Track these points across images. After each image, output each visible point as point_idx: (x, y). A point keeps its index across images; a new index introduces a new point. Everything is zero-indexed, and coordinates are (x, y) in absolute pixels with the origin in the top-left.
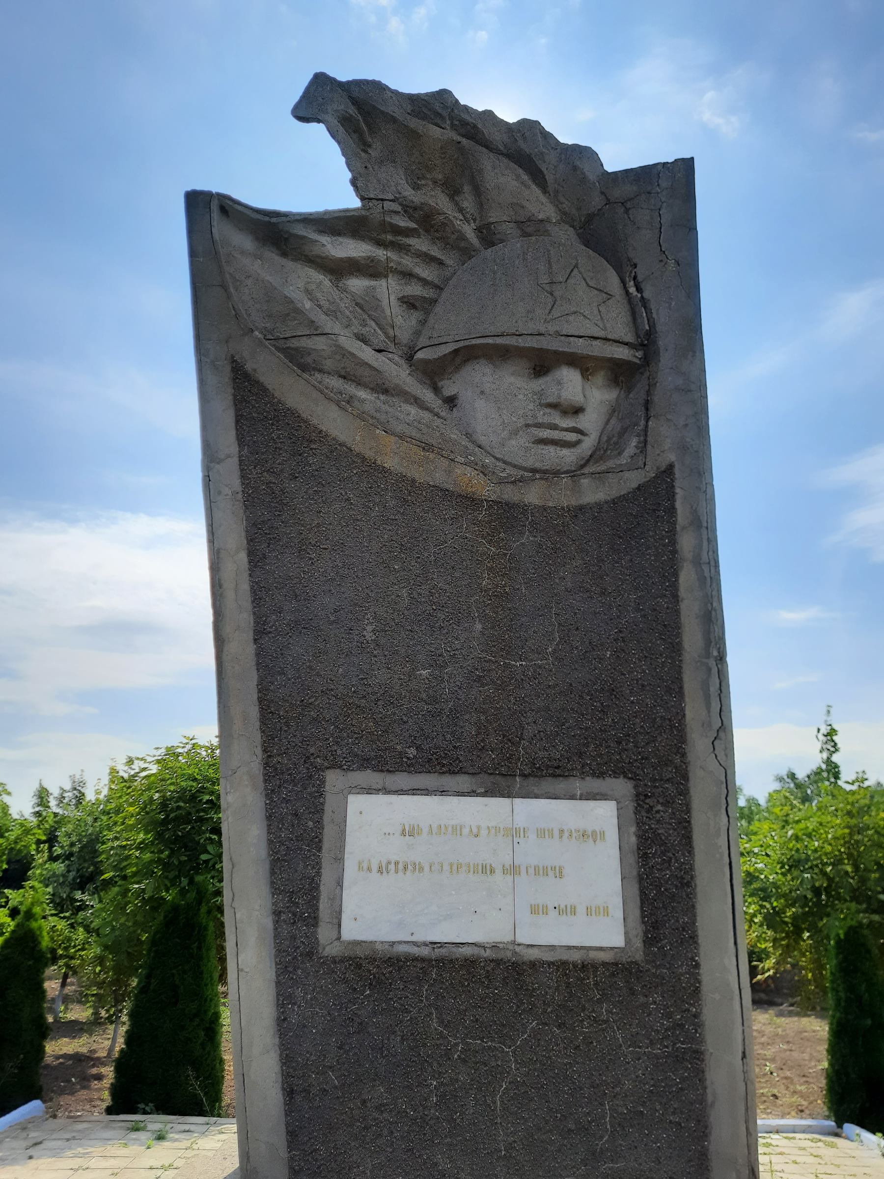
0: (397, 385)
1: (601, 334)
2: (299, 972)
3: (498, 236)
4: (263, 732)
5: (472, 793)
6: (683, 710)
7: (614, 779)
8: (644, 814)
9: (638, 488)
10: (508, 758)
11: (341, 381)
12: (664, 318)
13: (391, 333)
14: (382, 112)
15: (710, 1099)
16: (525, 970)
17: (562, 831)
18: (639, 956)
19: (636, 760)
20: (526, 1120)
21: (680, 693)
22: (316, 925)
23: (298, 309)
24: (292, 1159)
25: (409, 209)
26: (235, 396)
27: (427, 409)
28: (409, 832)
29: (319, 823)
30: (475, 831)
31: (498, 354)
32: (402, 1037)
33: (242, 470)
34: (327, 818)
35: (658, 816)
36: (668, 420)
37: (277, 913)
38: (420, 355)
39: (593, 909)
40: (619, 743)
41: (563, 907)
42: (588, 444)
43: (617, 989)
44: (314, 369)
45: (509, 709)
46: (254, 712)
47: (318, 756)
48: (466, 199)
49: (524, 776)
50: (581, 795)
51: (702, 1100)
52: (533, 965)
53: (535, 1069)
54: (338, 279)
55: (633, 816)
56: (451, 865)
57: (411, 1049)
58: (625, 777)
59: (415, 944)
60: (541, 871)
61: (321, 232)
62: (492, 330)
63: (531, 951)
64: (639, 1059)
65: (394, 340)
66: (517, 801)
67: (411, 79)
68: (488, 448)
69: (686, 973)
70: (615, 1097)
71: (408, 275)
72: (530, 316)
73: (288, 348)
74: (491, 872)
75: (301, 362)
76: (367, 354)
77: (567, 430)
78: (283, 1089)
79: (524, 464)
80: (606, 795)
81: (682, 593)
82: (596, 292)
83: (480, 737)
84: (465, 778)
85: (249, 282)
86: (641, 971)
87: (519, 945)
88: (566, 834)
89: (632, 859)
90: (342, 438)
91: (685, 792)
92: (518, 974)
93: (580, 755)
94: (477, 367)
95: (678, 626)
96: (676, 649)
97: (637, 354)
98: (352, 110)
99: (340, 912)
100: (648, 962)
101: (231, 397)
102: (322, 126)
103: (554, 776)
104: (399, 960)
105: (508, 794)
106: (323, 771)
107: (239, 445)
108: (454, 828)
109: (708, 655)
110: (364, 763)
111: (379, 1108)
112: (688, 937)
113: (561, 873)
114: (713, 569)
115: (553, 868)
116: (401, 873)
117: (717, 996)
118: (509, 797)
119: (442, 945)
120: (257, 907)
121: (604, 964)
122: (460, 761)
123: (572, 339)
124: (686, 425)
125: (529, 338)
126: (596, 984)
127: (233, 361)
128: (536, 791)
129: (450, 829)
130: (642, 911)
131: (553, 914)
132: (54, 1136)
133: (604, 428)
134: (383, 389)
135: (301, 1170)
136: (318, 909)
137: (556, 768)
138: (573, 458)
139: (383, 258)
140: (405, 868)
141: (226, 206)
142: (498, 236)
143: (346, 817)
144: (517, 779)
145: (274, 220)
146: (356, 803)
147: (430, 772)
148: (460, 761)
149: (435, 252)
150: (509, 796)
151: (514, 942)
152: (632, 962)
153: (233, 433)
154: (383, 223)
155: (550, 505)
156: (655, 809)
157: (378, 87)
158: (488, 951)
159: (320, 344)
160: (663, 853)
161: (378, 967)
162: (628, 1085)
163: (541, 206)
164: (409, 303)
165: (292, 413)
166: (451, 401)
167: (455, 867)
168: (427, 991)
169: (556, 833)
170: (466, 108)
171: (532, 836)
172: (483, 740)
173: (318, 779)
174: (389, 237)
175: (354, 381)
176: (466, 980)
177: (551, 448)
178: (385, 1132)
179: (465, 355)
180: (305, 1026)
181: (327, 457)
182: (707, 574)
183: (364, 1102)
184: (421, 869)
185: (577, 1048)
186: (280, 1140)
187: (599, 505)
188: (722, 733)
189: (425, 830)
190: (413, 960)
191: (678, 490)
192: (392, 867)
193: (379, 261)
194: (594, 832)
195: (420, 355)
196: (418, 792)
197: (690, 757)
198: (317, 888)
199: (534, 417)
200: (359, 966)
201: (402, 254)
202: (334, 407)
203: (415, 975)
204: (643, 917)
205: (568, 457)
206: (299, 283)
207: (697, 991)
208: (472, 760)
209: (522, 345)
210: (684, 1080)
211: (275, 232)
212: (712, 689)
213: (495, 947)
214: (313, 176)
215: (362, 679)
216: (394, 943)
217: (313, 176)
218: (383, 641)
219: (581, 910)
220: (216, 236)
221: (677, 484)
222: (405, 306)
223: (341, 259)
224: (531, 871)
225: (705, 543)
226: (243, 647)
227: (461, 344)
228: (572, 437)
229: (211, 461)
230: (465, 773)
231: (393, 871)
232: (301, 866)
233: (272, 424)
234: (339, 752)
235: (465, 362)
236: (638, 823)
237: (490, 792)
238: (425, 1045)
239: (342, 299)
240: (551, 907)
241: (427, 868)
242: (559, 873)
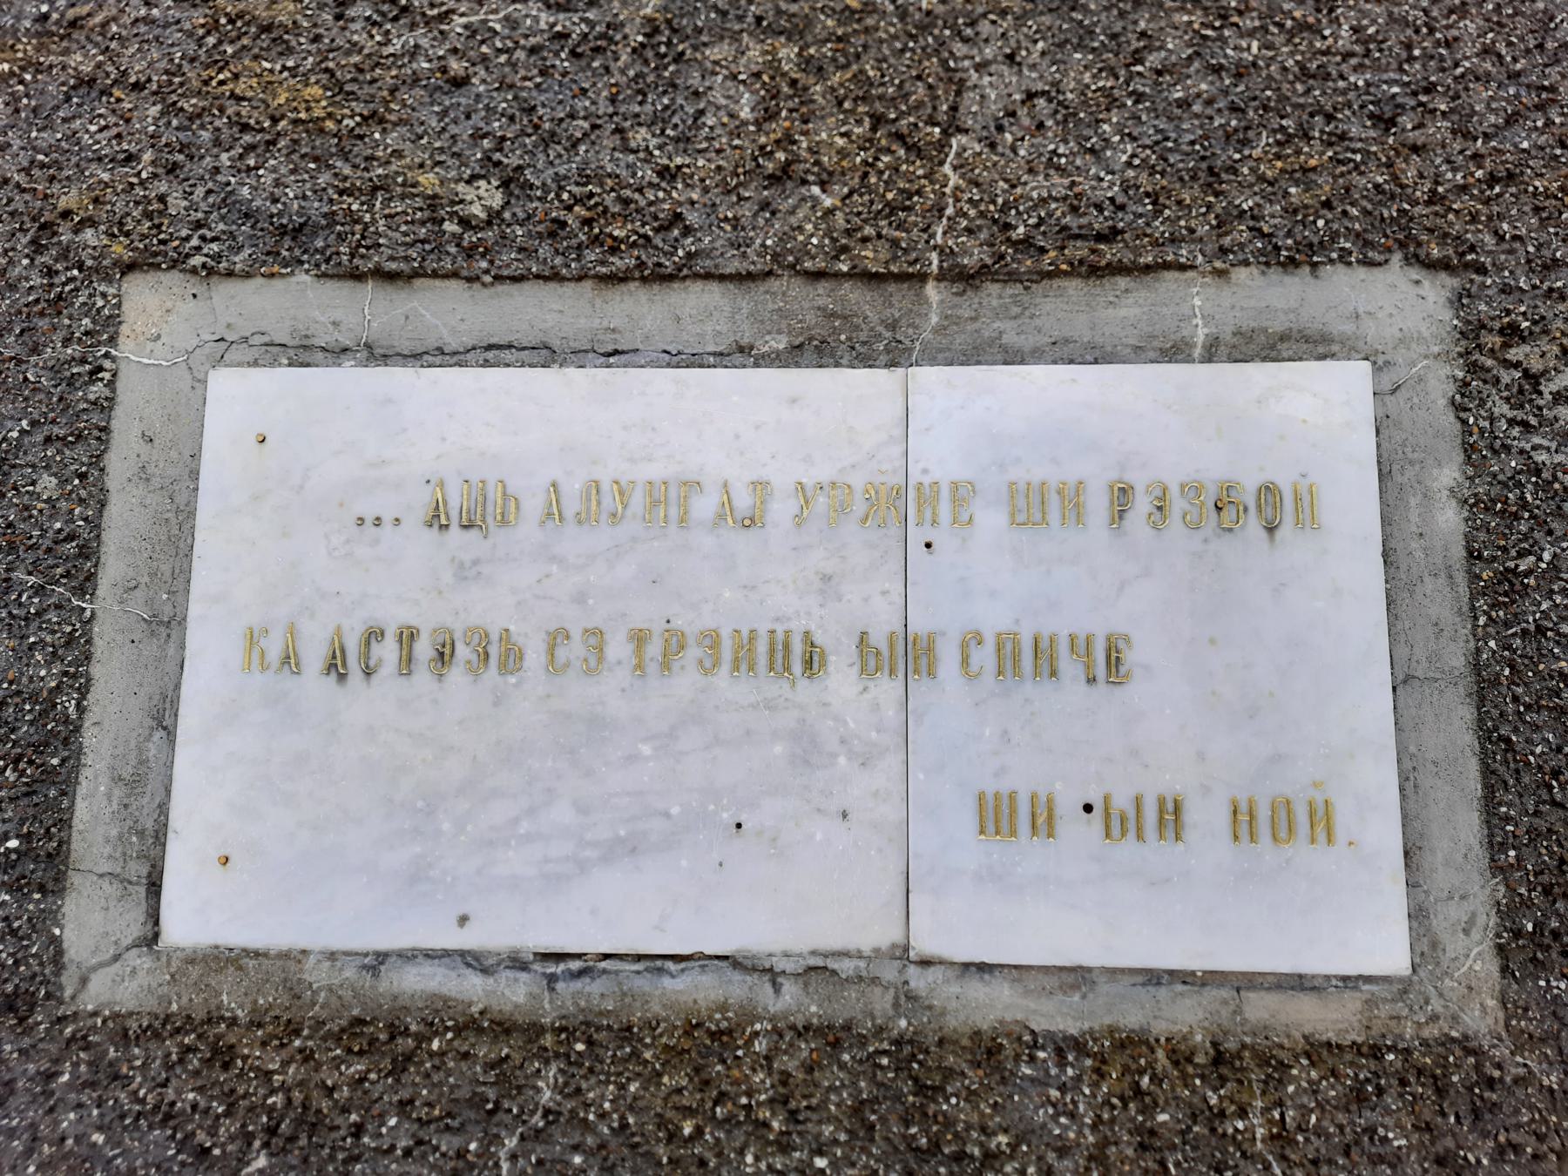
5: (742, 354)
7: (1362, 272)
10: (892, 208)
16: (949, 1074)
17: (1122, 496)
18: (1481, 1018)
19: (1464, 189)
28: (465, 514)
29: (89, 484)
30: (743, 501)
34: (119, 464)
39: (1263, 814)
40: (1386, 123)
41: (1122, 801)
47: (91, 222)
49: (964, 278)
52: (990, 1051)
56: (639, 638)
59: (473, 960)
60: (1028, 659)
63: (977, 990)
66: (927, 377)
74: (809, 663)
80: (1326, 339)
83: (777, 129)
84: (713, 294)
86: (1491, 1083)
87: (925, 963)
88: (1142, 505)
89: (1443, 603)
92: (920, 1089)
93: (1213, 178)
99: (160, 836)
103: (1094, 271)
104: (395, 1031)
105: (892, 350)
106: (108, 279)
108: (657, 496)
110: (289, 243)
113: (1114, 661)
115: (1081, 646)
118: (892, 364)
119: (587, 966)
121: (1317, 1051)
122: (688, 231)
126: (1281, 1138)
128: (1010, 338)
129: (638, 500)
131: (1079, 833)
136: (65, 823)
137: (1100, 238)
140: (444, 656)
143: (195, 456)
144: (932, 290)
147: (555, 277)
148: (688, 231)
150: (896, 357)
151: (901, 953)
158: (790, 990)
161: (307, 1056)
167: (654, 649)
168: (513, 1157)
169: (1098, 505)
171: (991, 519)
172: (787, 140)
173: (88, 309)
176: (688, 1112)
184: (512, 659)
189: (533, 505)
190: (458, 1030)
192: (387, 652)
194: (1268, 491)
196: (507, 355)
200: (223, 1056)
203: (464, 1093)
204: (1495, 846)
208: (735, 222)
213: (817, 972)
216: (382, 957)
219: (1207, 818)
224: (984, 657)
230: (708, 276)
234: (177, 204)
236: (1469, 449)
237: (812, 349)
240: (1068, 805)
241: (535, 657)
242: (1111, 663)
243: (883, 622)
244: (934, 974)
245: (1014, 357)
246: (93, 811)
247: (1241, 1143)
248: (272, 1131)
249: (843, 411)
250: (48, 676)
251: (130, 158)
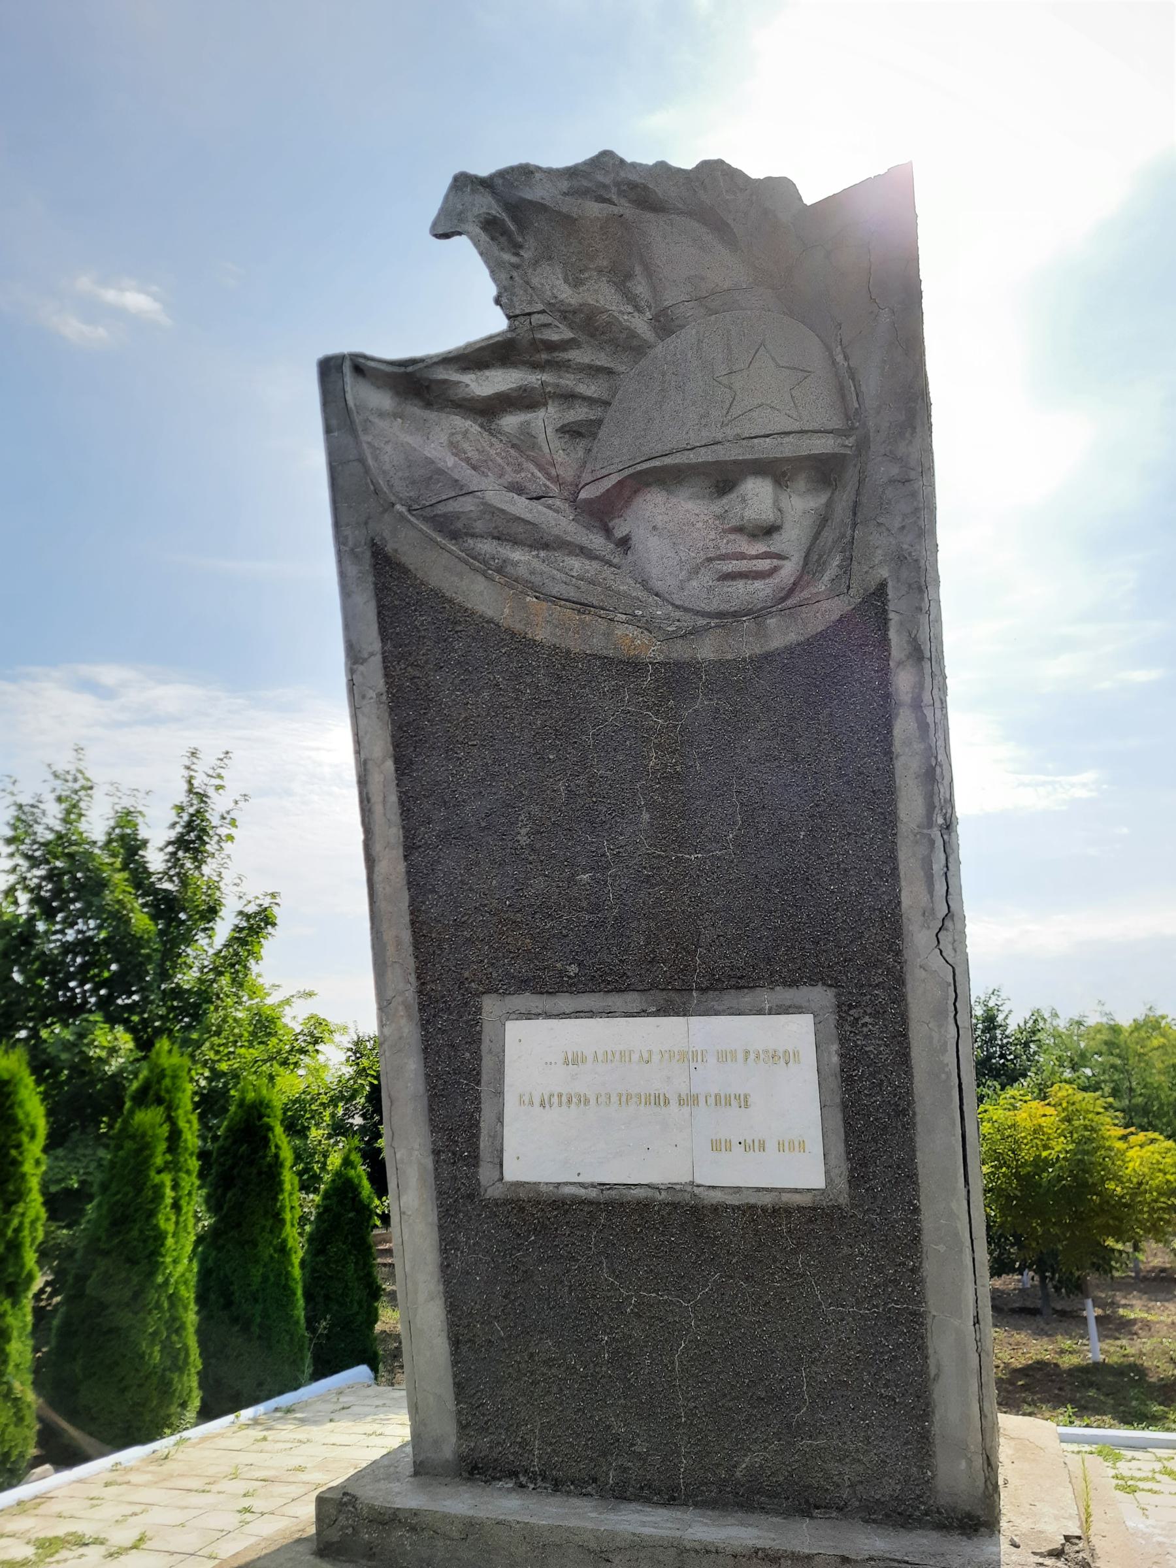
0: (557, 537)
1: (796, 426)
2: (461, 1215)
3: (677, 322)
4: (416, 957)
5: (642, 1013)
6: (898, 896)
8: (848, 1028)
9: (840, 620)
10: (682, 970)
11: (495, 542)
13: (553, 472)
14: (530, 202)
15: (933, 1371)
18: (843, 1200)
20: (709, 1384)
21: (895, 873)
22: (476, 1165)
23: (439, 469)
24: (459, 1412)
25: (566, 314)
26: (375, 584)
27: (596, 558)
28: (574, 1060)
30: (646, 1056)
31: (667, 477)
32: (570, 1287)
33: (385, 668)
35: (865, 1029)
36: (879, 524)
37: (436, 1153)
38: (583, 495)
39: (786, 1144)
42: (789, 570)
43: (815, 1238)
44: (466, 534)
45: (683, 912)
46: (407, 936)
48: (640, 283)
49: (703, 990)
50: (770, 1009)
51: (923, 1372)
52: (716, 1209)
53: (718, 1328)
54: (490, 421)
55: (835, 1030)
56: (620, 1095)
57: (580, 1300)
58: (824, 984)
59: (582, 1185)
60: (721, 1101)
61: (465, 369)
62: (660, 448)
63: (712, 1193)
64: (842, 1320)
65: (557, 480)
66: (693, 1020)
67: (562, 150)
68: (667, 596)
69: (902, 1219)
70: (813, 1362)
71: (569, 398)
72: (703, 422)
73: (436, 516)
75: (451, 528)
76: (520, 506)
77: (757, 557)
78: (449, 1338)
79: (707, 609)
80: (801, 1007)
81: (897, 747)
82: (788, 372)
84: (635, 995)
85: (389, 448)
87: (698, 1186)
88: (752, 1056)
89: (834, 1083)
90: (490, 613)
91: (899, 998)
93: (769, 961)
94: (649, 496)
95: (891, 790)
96: (889, 820)
97: (847, 443)
98: (504, 213)
99: (502, 1151)
100: (854, 1206)
101: (372, 587)
102: (464, 238)
104: (564, 1204)
107: (382, 641)
109: (930, 824)
111: (548, 1363)
112: (906, 1176)
114: (938, 712)
116: (564, 1107)
117: (942, 1248)
119: (612, 1186)
120: (417, 1146)
121: (800, 1209)
123: (756, 441)
124: (903, 527)
125: (703, 450)
127: (373, 544)
129: (617, 1055)
130: (847, 1145)
132: (366, 1402)
133: (813, 544)
134: (542, 543)
135: (468, 1424)
138: (768, 591)
139: (537, 385)
140: (569, 1101)
141: (360, 366)
142: (677, 322)
144: (694, 994)
145: (410, 369)
146: (515, 1031)
149: (602, 360)
151: (692, 1183)
152: (834, 1206)
153: (375, 627)
154: (533, 342)
155: (729, 657)
156: (860, 1022)
157: (526, 172)
159: (467, 505)
160: (873, 1075)
162: (830, 1350)
164: (572, 432)
165: (437, 594)
166: (624, 543)
167: (624, 1099)
169: (740, 1056)
170: (634, 165)
171: (712, 1060)
172: (653, 951)
173: (474, 1006)
174: (544, 356)
175: (508, 541)
176: (639, 1226)
177: (740, 584)
178: (555, 1389)
179: (641, 480)
180: (468, 1273)
181: (474, 638)
182: (930, 720)
183: (531, 1355)
184: (587, 1102)
185: (767, 1304)
186: (447, 1391)
187: (790, 650)
188: (949, 920)
189: (590, 1059)
191: (892, 615)
192: (555, 1100)
193: (533, 389)
195: (583, 495)
197: (908, 954)
198: (477, 1125)
199: (717, 547)
201: (562, 373)
202: (481, 578)
205: (762, 589)
206: (439, 440)
207: (916, 1240)
209: (694, 461)
210: (898, 1346)
211: (417, 384)
212: (935, 867)
213: (670, 1188)
214: (455, 303)
215: (517, 890)
217: (455, 303)
218: (538, 845)
219: (771, 1145)
220: (351, 403)
221: (891, 606)
222: (567, 436)
223: (489, 398)
224: (712, 1100)
225: (928, 679)
226: (393, 865)
227: (626, 473)
229: (354, 663)
231: (556, 1104)
232: (460, 1101)
233: (416, 610)
234: (495, 975)
235: (635, 492)
237: (663, 1011)
238: (593, 1296)
239: (492, 445)
240: (735, 1143)
241: (593, 1101)
243: (684, 1091)
244: (701, 1189)
245: (717, 1013)
246: (484, 1143)
247: (780, 1232)
248: (535, 1229)
249: (533, 1520)
250: (472, 1108)
251: (482, 961)
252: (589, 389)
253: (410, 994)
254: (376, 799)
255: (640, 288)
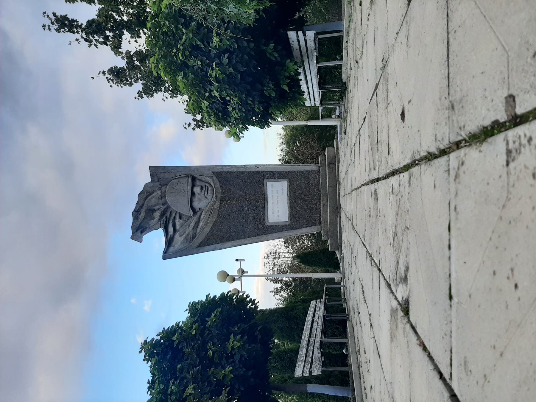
12: (182, 173)
71: (175, 218)
76: (192, 225)
98: (139, 230)
110: (264, 220)
141: (165, 252)
159: (192, 233)
163: (158, 193)
165: (206, 236)
206: (179, 240)
211: (169, 242)
214: (156, 238)
217: (156, 238)
228: (206, 188)
252: (173, 215)
253: (265, 236)
254: (237, 243)
255: (157, 207)
